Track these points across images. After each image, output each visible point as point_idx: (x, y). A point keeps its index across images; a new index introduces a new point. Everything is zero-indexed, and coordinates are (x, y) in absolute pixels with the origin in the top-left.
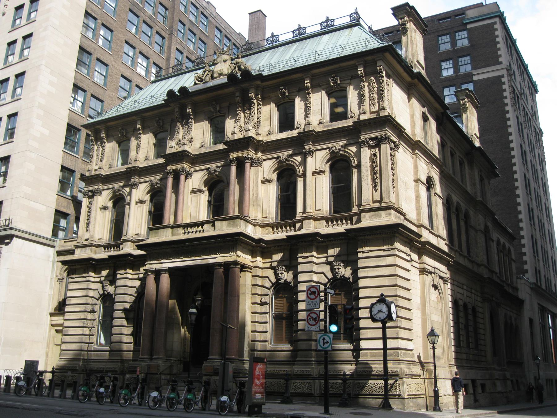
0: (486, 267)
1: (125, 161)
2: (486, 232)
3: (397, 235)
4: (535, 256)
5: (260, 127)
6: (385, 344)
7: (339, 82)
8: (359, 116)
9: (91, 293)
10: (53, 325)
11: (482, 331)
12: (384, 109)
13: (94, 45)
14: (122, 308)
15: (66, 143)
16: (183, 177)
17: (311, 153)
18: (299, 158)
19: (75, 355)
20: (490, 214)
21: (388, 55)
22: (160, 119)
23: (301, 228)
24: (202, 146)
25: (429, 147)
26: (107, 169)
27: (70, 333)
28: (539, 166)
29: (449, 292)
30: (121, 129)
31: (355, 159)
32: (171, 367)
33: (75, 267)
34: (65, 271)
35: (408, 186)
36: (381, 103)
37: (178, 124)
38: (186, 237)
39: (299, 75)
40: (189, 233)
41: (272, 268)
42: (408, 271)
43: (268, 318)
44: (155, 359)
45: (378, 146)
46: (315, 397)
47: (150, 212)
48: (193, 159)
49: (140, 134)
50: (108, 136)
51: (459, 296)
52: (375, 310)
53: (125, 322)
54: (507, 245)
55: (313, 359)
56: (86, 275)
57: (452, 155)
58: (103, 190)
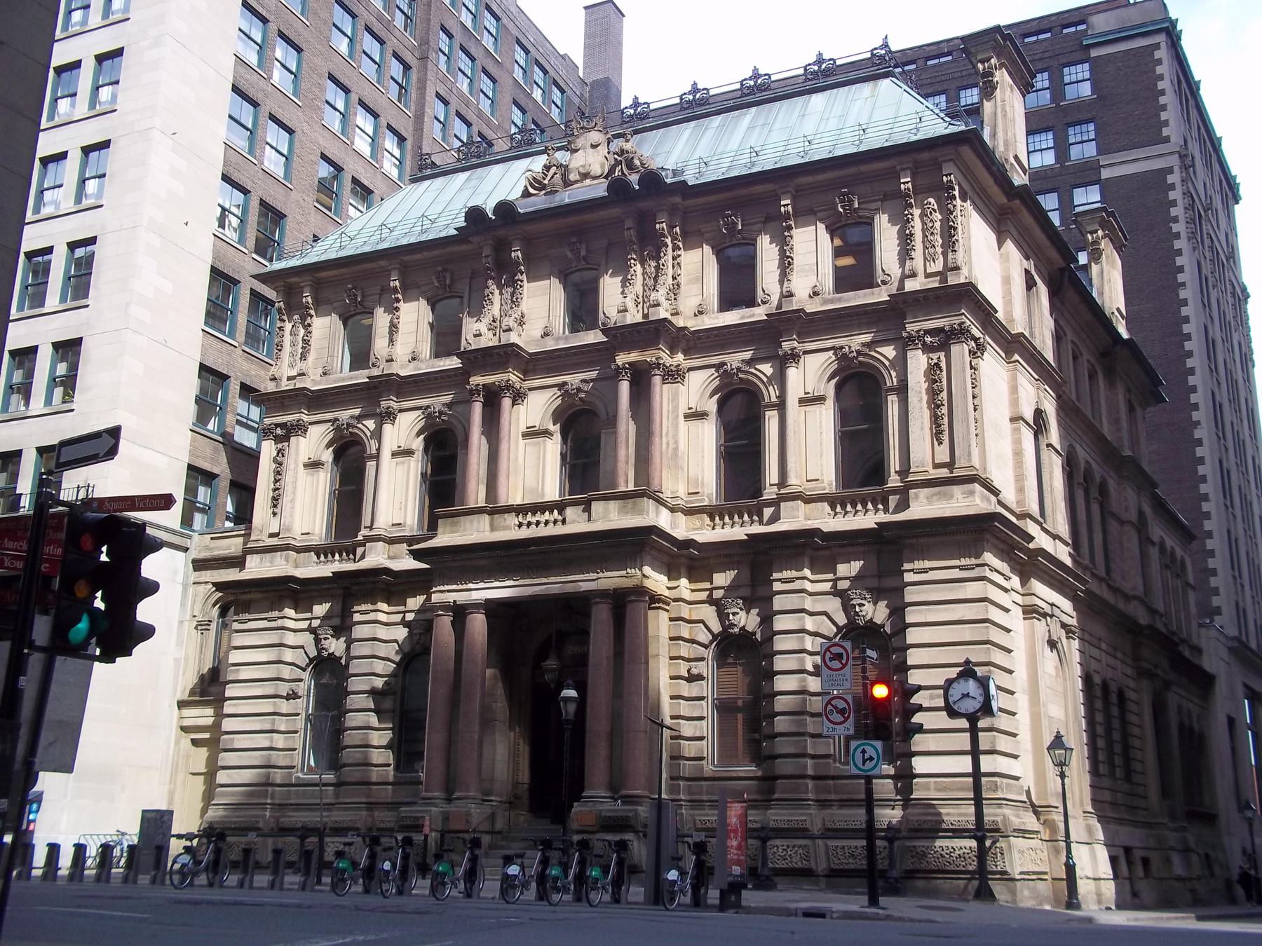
0: (1141, 601)
1: (361, 357)
2: (1141, 526)
3: (988, 536)
4: (1234, 577)
5: (679, 298)
6: (976, 764)
7: (856, 206)
8: (902, 281)
9: (288, 656)
10: (184, 729)
11: (1136, 743)
12: (957, 268)
13: (262, 83)
14: (367, 688)
15: (208, 314)
16: (507, 402)
17: (794, 357)
18: (767, 368)
19: (251, 794)
20: (1146, 484)
21: (966, 151)
22: (445, 270)
23: (775, 518)
24: (546, 335)
25: (1037, 343)
26: (318, 378)
27: (237, 746)
28: (1240, 372)
29: (1076, 657)
30: (352, 287)
31: (894, 374)
32: (492, 817)
33: (248, 597)
34: (214, 605)
35: (999, 432)
36: (950, 255)
37: (490, 282)
38: (524, 533)
39: (768, 187)
40: (529, 524)
41: (711, 601)
42: (1007, 610)
43: (705, 708)
44: (457, 799)
45: (944, 346)
46: (818, 876)
47: (423, 475)
48: (528, 362)
49: (398, 300)
50: (318, 303)
51: (1094, 665)
52: (956, 692)
53: (373, 720)
54: (1179, 552)
55: (810, 796)
56: (276, 614)
57: (1075, 358)
58: (311, 424)
